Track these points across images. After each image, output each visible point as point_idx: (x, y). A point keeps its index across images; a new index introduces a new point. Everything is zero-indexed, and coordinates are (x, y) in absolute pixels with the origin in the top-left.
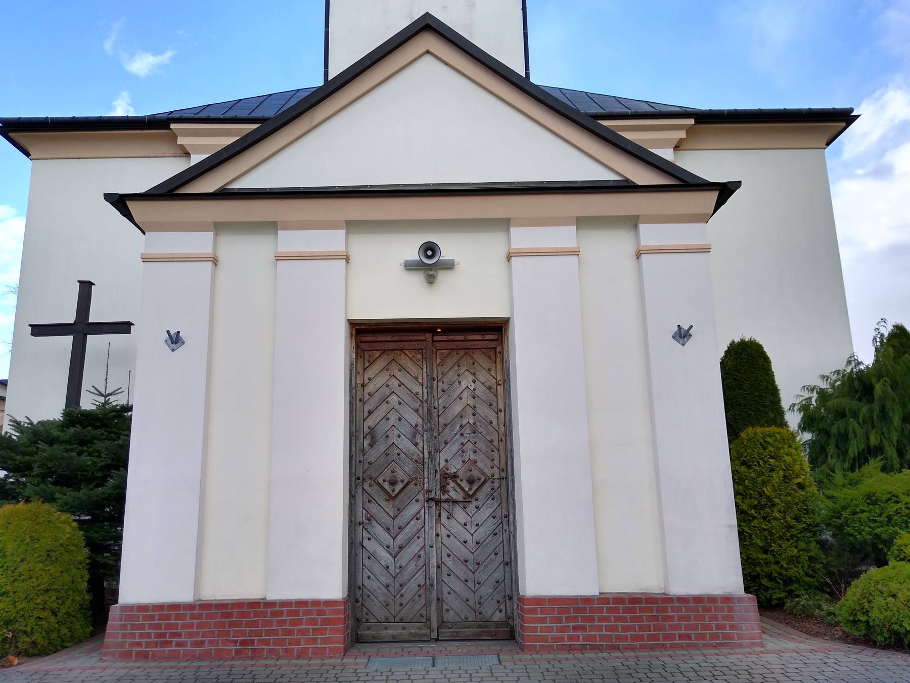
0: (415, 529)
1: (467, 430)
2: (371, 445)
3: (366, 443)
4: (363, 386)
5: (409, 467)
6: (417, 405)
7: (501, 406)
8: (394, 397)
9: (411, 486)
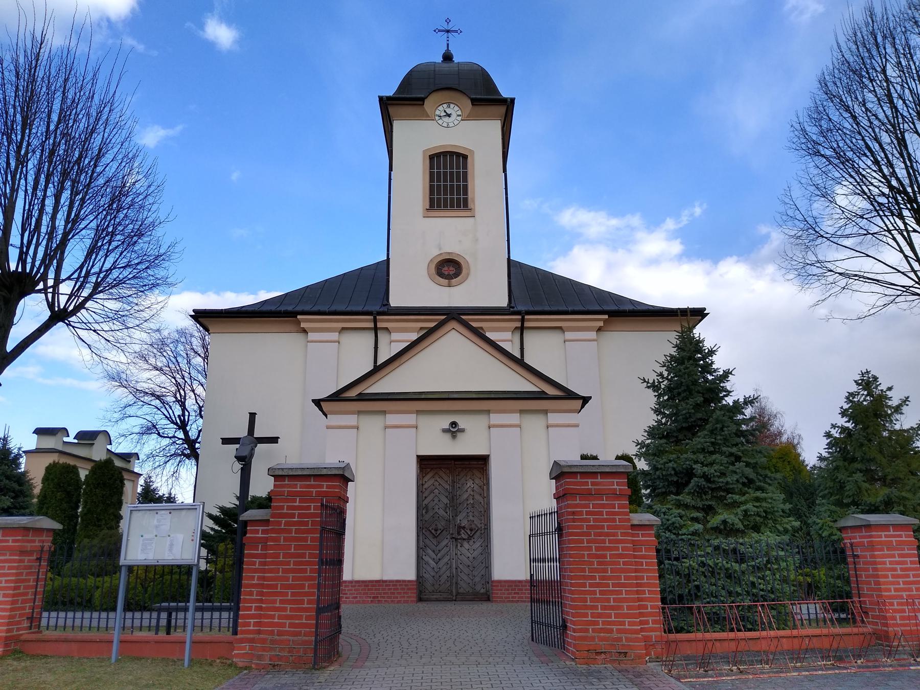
0: (446, 552)
1: (470, 506)
2: (426, 513)
3: (424, 511)
4: (423, 485)
5: (443, 523)
6: (447, 494)
7: (485, 495)
8: (436, 490)
9: (444, 532)
